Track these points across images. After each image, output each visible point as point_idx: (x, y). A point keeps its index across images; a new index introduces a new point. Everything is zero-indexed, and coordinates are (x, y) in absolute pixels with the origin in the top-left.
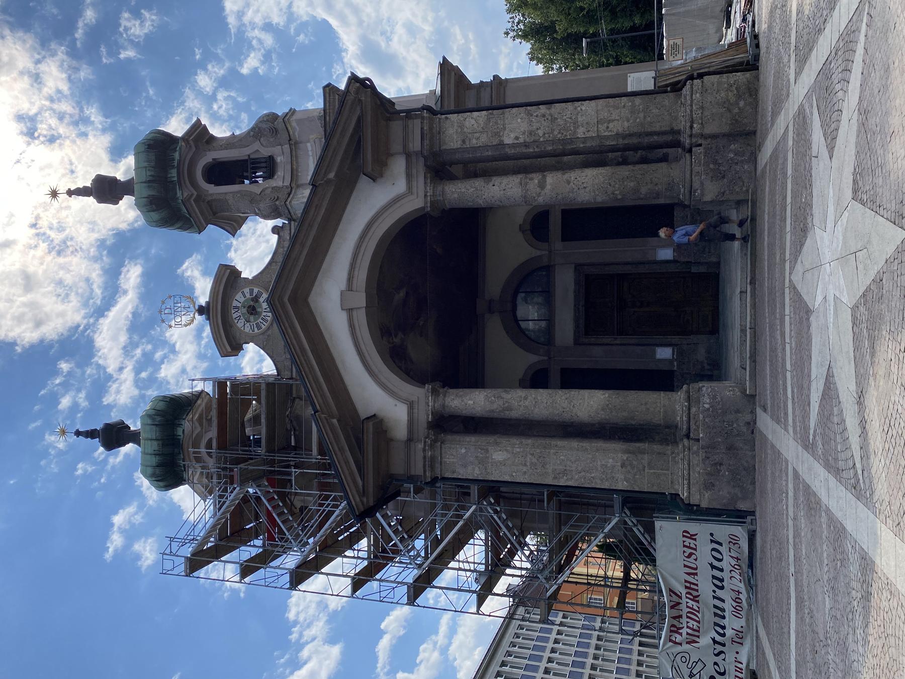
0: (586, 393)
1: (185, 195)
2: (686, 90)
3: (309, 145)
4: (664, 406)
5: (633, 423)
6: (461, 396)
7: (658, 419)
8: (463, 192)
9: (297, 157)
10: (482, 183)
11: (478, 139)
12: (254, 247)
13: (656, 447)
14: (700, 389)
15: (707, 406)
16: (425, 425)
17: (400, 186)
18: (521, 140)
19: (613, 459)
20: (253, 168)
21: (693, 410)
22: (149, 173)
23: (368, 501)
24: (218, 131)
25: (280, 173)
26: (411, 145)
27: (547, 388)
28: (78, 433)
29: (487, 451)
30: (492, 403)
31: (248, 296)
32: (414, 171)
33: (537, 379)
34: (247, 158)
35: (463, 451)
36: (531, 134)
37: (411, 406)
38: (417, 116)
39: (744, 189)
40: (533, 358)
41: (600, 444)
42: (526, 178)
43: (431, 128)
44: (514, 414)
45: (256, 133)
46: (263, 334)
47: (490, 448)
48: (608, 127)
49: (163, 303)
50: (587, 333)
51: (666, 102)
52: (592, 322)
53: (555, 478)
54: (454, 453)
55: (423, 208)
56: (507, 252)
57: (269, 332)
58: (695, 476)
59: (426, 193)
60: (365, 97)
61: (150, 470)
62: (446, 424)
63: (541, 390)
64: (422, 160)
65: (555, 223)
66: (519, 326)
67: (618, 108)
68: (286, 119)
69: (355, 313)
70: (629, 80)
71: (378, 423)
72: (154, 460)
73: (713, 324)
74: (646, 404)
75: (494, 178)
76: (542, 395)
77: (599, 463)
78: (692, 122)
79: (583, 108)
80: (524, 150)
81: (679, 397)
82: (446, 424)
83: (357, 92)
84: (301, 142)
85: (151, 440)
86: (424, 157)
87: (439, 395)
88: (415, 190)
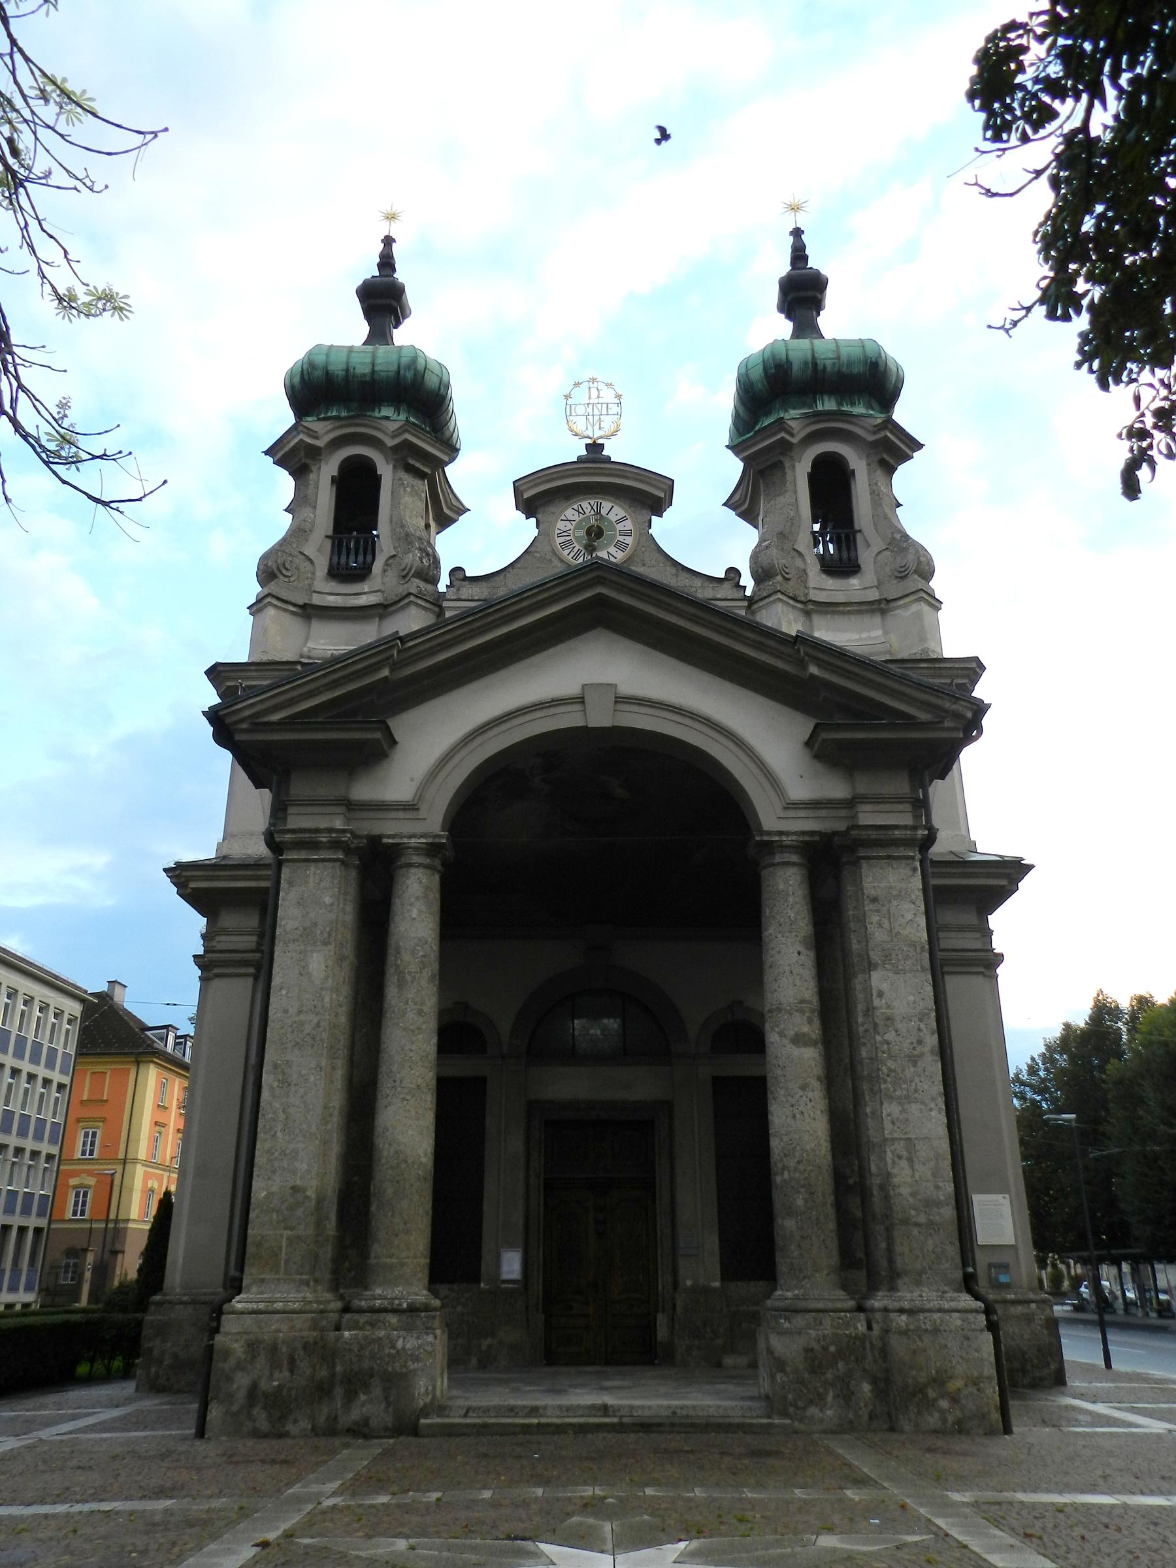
0: (429, 1119)
1: (792, 424)
3: (879, 632)
5: (373, 1208)
6: (426, 896)
7: (379, 1252)
8: (787, 896)
9: (859, 612)
11: (880, 925)
12: (706, 537)
14: (429, 1329)
15: (400, 1344)
17: (799, 790)
19: (308, 1171)
21: (393, 1319)
22: (828, 363)
24: (906, 480)
25: (830, 583)
26: (869, 807)
30: (413, 953)
31: (619, 527)
32: (823, 813)
33: (456, 1034)
34: (857, 527)
35: (328, 900)
36: (888, 1019)
37: (409, 807)
38: (917, 817)
41: (336, 1148)
42: (813, 1011)
44: (391, 992)
45: (900, 542)
46: (554, 553)
47: (332, 947)
48: (900, 1157)
49: (609, 385)
51: (945, 1265)
53: (276, 1066)
54: (323, 884)
59: (787, 834)
61: (320, 359)
63: (435, 1040)
64: (841, 826)
65: (739, 1066)
67: (934, 1175)
68: (923, 594)
70: (999, 1198)
71: (375, 752)
72: (337, 366)
75: (812, 954)
77: (300, 1146)
79: (933, 1113)
80: (860, 1007)
81: (419, 1293)
82: (375, 869)
83: (957, 716)
85: (373, 364)
86: (849, 829)
88: (791, 814)
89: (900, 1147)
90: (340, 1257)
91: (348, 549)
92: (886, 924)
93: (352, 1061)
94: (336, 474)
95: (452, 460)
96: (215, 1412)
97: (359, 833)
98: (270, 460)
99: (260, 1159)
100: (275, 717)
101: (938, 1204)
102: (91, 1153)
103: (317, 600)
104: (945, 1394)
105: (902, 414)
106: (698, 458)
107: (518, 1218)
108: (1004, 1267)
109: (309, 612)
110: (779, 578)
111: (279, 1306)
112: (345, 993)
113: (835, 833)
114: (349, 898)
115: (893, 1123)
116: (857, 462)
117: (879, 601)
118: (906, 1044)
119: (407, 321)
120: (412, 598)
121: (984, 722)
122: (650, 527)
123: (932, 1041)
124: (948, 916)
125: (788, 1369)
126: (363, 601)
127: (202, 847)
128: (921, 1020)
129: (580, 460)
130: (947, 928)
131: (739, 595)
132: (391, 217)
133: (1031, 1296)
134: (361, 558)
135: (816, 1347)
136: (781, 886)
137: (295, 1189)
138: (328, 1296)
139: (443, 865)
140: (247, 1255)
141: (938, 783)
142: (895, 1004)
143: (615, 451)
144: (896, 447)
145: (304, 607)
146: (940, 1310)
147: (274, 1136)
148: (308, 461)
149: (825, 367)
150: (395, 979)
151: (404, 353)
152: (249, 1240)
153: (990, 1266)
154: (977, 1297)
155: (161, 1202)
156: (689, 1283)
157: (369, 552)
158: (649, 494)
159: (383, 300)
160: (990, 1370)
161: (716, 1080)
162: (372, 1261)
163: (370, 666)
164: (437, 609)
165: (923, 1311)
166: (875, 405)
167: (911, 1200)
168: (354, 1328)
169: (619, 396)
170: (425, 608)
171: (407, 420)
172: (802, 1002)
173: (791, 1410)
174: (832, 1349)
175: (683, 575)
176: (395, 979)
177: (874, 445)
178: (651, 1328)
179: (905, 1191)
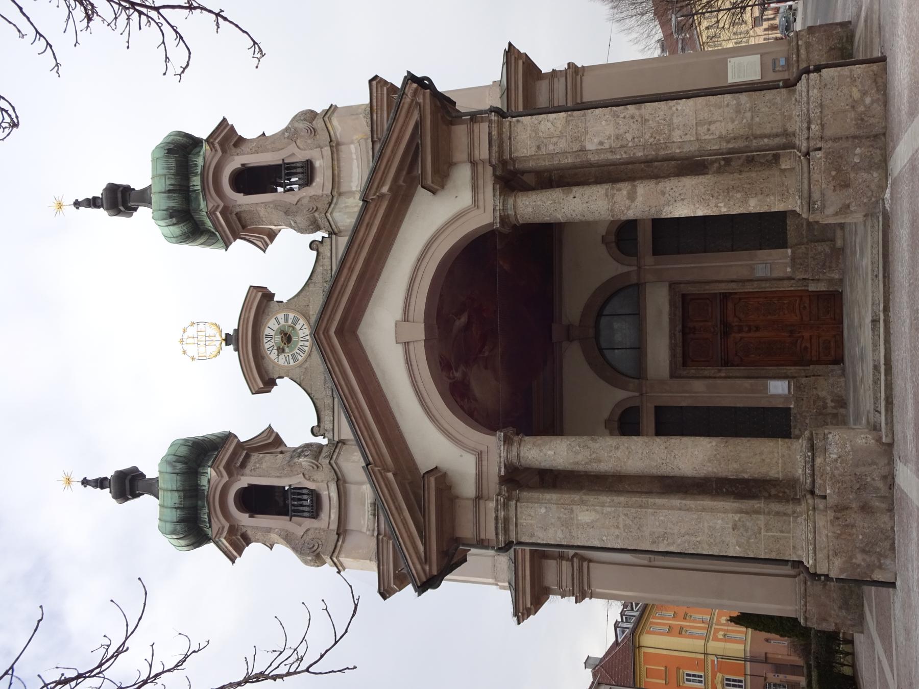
1: (210, 206)
2: (801, 86)
3: (352, 146)
5: (746, 476)
7: (775, 472)
8: (535, 206)
9: (338, 160)
10: (561, 195)
11: (555, 144)
12: (287, 262)
13: (775, 507)
14: (825, 437)
16: (497, 480)
18: (607, 146)
19: (723, 519)
21: (818, 461)
22: (168, 182)
23: (430, 569)
25: (318, 180)
26: (477, 152)
27: (637, 434)
28: (85, 482)
29: (572, 511)
30: (576, 453)
31: (282, 322)
32: (481, 182)
33: (626, 424)
34: (281, 162)
35: (543, 511)
37: (479, 457)
39: (873, 199)
40: (621, 395)
41: (708, 503)
42: (613, 188)
43: (500, 134)
45: (290, 133)
46: (300, 366)
48: (709, 130)
49: (185, 331)
50: (684, 364)
51: (778, 100)
52: (690, 355)
54: (533, 514)
56: (587, 273)
57: (307, 365)
58: (822, 540)
59: (495, 206)
60: (424, 98)
62: (518, 479)
64: (490, 170)
65: (645, 237)
66: (603, 356)
69: (411, 346)
70: (729, 65)
71: (442, 479)
72: (174, 515)
73: (833, 354)
75: (575, 189)
76: (636, 444)
77: (706, 524)
78: (809, 123)
79: (679, 108)
80: (610, 157)
82: (518, 479)
84: (343, 144)
85: (171, 491)
87: (512, 445)
88: (481, 203)
89: (702, 130)
90: (779, 499)
91: (297, 506)
92: (555, 140)
93: (649, 493)
94: (247, 515)
95: (236, 437)
96: (878, 576)
97: (498, 491)
98: (238, 560)
99: (715, 551)
100: (421, 548)
101: (739, 104)
102: (701, 676)
103: (334, 526)
104: (862, 100)
105: (202, 132)
106: (228, 273)
107: (747, 383)
108: (775, 62)
109: (342, 531)
110: (316, 214)
111: (810, 536)
112: (605, 498)
113: (494, 175)
114: (541, 496)
115: (686, 134)
116: (236, 162)
117: (331, 147)
118: (634, 126)
119: (140, 469)
120: (332, 462)
121: (419, 76)
122: (281, 302)
123: (631, 109)
124: (542, 100)
125: (847, 202)
126: (334, 495)
127: (504, 598)
128: (618, 117)
129: (237, 349)
130: (551, 100)
131: (328, 240)
132: (69, 481)
133: (794, 43)
134: (305, 497)
135: (833, 183)
136: (530, 210)
137: (734, 528)
138: (804, 505)
139: (518, 434)
140: (778, 558)
142: (607, 133)
143: (230, 326)
144: (226, 136)
145: (338, 534)
147: (699, 542)
148: (239, 534)
149: (171, 185)
150: (595, 465)
151: (164, 470)
152: (767, 557)
153: (774, 71)
154: (799, 79)
155: (737, 623)
156: (789, 270)
157: (300, 491)
158: (261, 301)
159: (128, 484)
160: (846, 70)
161: (655, 253)
162: (781, 476)
163: (386, 485)
164: (340, 444)
165: (808, 114)
166: (197, 149)
167: (736, 122)
168: (825, 486)
169: (193, 324)
170: (339, 453)
171: (211, 467)
172: (607, 196)
173: (873, 199)
174: (834, 173)
175: (314, 278)
176: (595, 465)
177: (224, 151)
178: (818, 295)
179: (730, 126)
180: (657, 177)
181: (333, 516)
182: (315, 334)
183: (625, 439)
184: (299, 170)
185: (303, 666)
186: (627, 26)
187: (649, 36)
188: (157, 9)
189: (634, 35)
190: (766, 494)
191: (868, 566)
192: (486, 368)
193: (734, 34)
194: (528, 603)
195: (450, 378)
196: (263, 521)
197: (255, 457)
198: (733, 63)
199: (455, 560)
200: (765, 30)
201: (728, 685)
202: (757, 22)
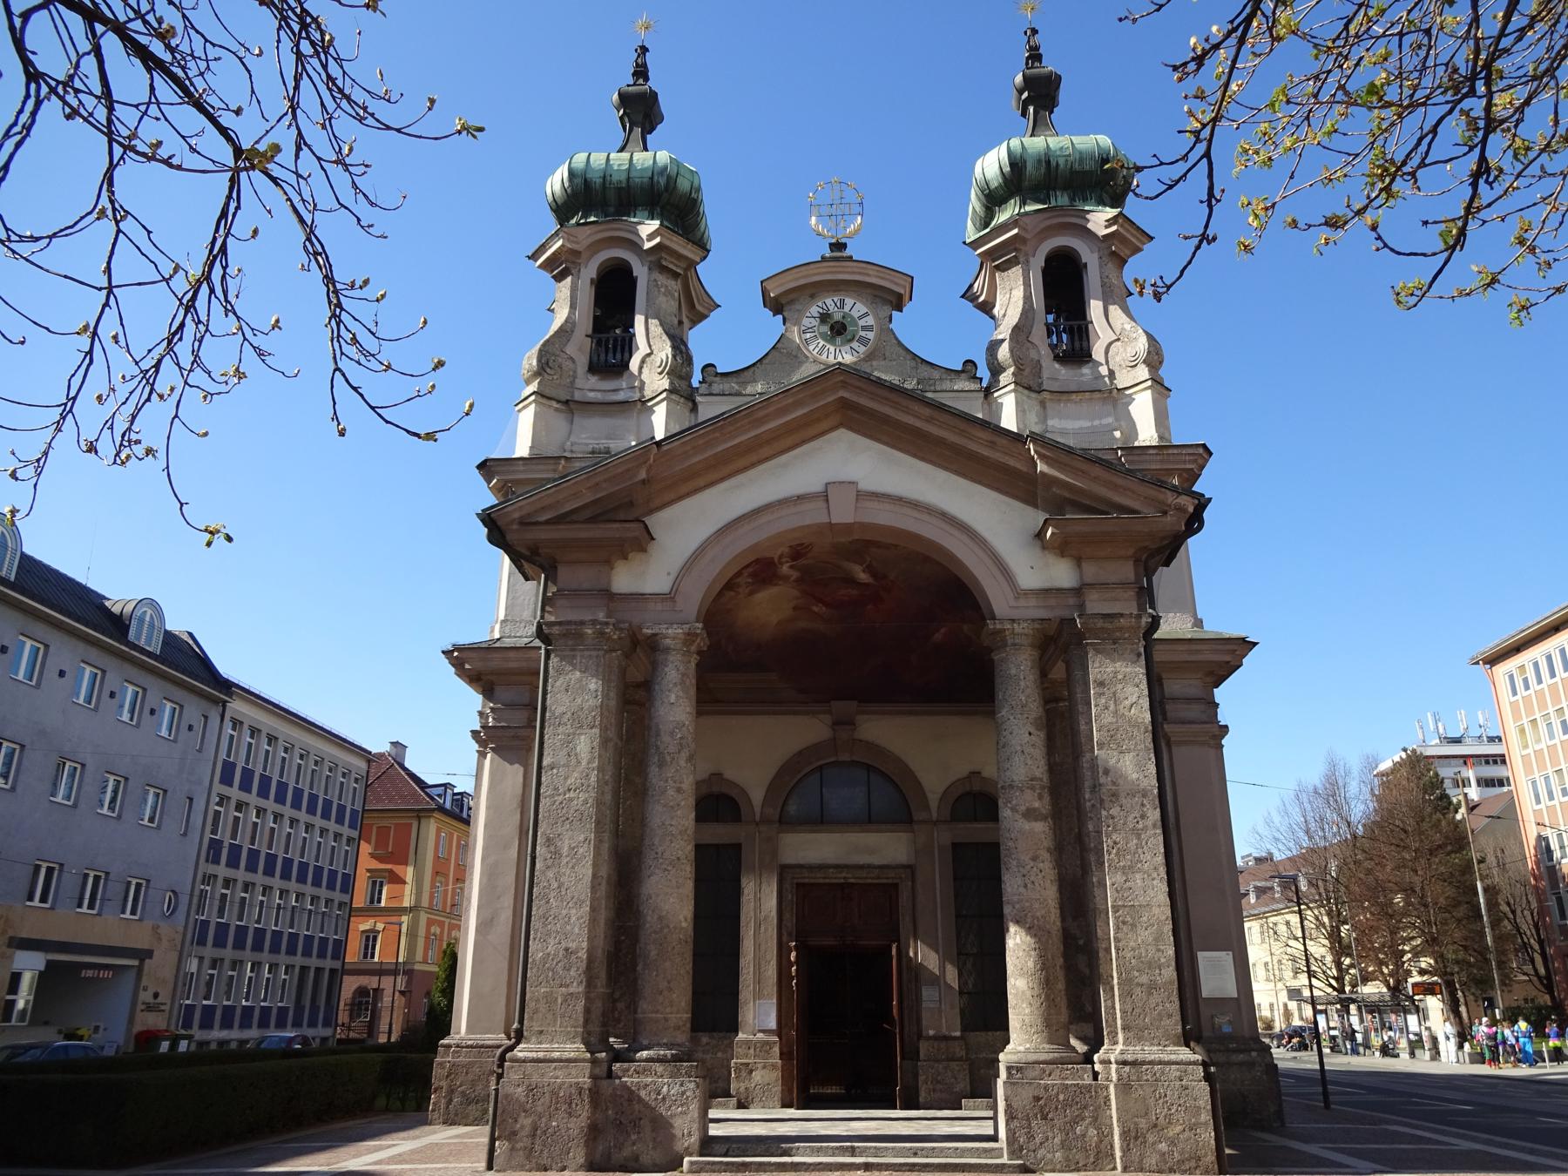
0: (689, 887)
4: (666, 1020)
5: (639, 968)
6: (683, 682)
8: (1019, 677)
10: (1034, 715)
18: (1102, 780)
20: (1071, 328)
22: (1061, 161)
27: (698, 819)
31: (862, 323)
32: (1052, 602)
33: (716, 803)
37: (669, 597)
38: (1141, 608)
40: (757, 796)
42: (1043, 788)
55: (993, 618)
56: (930, 750)
60: (1174, 522)
65: (975, 831)
71: (643, 541)
74: (670, 989)
75: (1042, 735)
84: (1115, 406)
88: (1022, 602)
92: (1112, 707)
103: (578, 396)
121: (1205, 515)
134: (619, 356)
136: (1013, 672)
141: (1162, 571)
145: (567, 402)
146: (1160, 1063)
156: (931, 1033)
158: (891, 295)
175: (924, 367)
180: (1058, 851)
181: (592, 394)
182: (840, 368)
183: (692, 801)
184: (1077, 344)
185: (344, 364)
186: (1290, 809)
187: (1277, 840)
188: (1207, 155)
189: (1277, 819)
190: (617, 995)
191: (514, 1133)
192: (795, 608)
193: (1280, 962)
194: (472, 664)
195: (781, 557)
196: (587, 295)
197: (675, 286)
198: (1226, 958)
199: (526, 565)
200: (1285, 1005)
201: (368, 938)
202: (1294, 994)
